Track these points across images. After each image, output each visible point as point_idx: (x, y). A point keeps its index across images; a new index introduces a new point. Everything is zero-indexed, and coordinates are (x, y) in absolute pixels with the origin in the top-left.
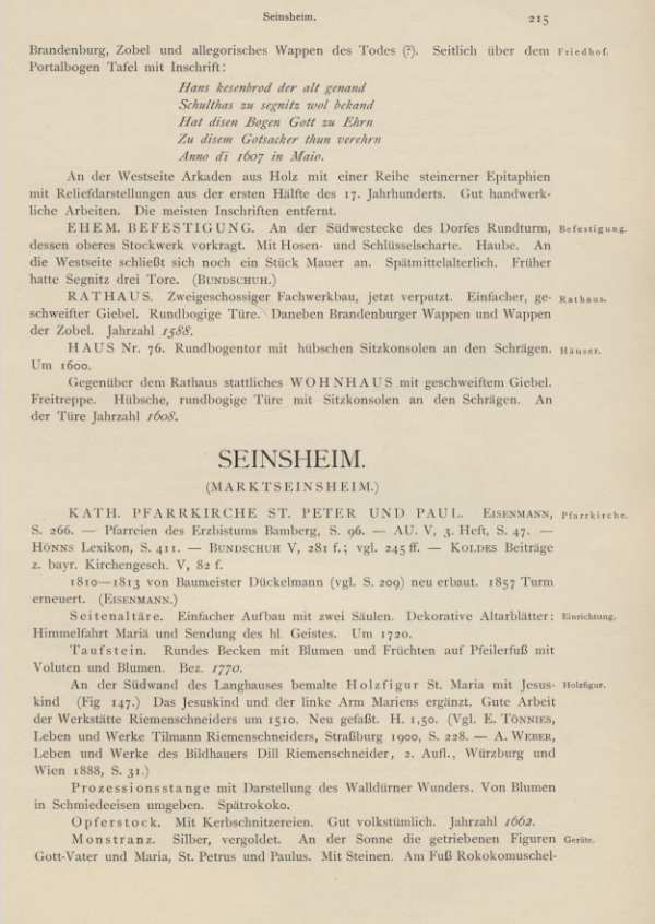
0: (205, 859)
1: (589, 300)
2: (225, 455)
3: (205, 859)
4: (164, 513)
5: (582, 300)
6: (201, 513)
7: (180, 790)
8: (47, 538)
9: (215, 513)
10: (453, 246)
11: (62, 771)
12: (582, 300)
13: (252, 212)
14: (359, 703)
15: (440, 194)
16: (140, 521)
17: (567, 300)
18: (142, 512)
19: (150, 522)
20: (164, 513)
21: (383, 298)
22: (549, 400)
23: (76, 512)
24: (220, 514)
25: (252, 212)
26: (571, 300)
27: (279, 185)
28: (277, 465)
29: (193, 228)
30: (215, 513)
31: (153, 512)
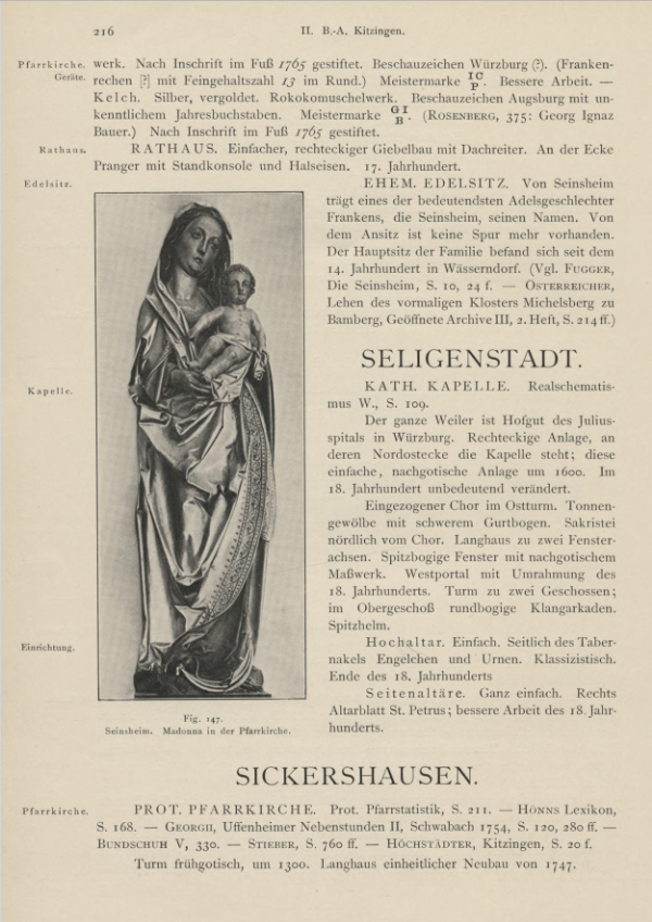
0: (415, 712)
1: (69, 151)
2: (242, 772)
3: (415, 712)
4: (220, 810)
5: (62, 150)
6: (256, 809)
7: (410, 644)
8: (110, 836)
9: (270, 810)
10: (571, 218)
11: (354, 677)
12: (62, 150)
13: (209, 65)
14: (523, 219)
15: (378, 729)
16: (196, 819)
17: (46, 150)
18: (199, 808)
19: (207, 819)
20: (220, 810)
21: (352, 627)
22: (611, 473)
23: (435, 385)
24: (276, 810)
25: (209, 65)
26: (50, 151)
27: (535, 311)
28: (484, 364)
29: (165, 149)
30: (270, 810)
31: (209, 809)
